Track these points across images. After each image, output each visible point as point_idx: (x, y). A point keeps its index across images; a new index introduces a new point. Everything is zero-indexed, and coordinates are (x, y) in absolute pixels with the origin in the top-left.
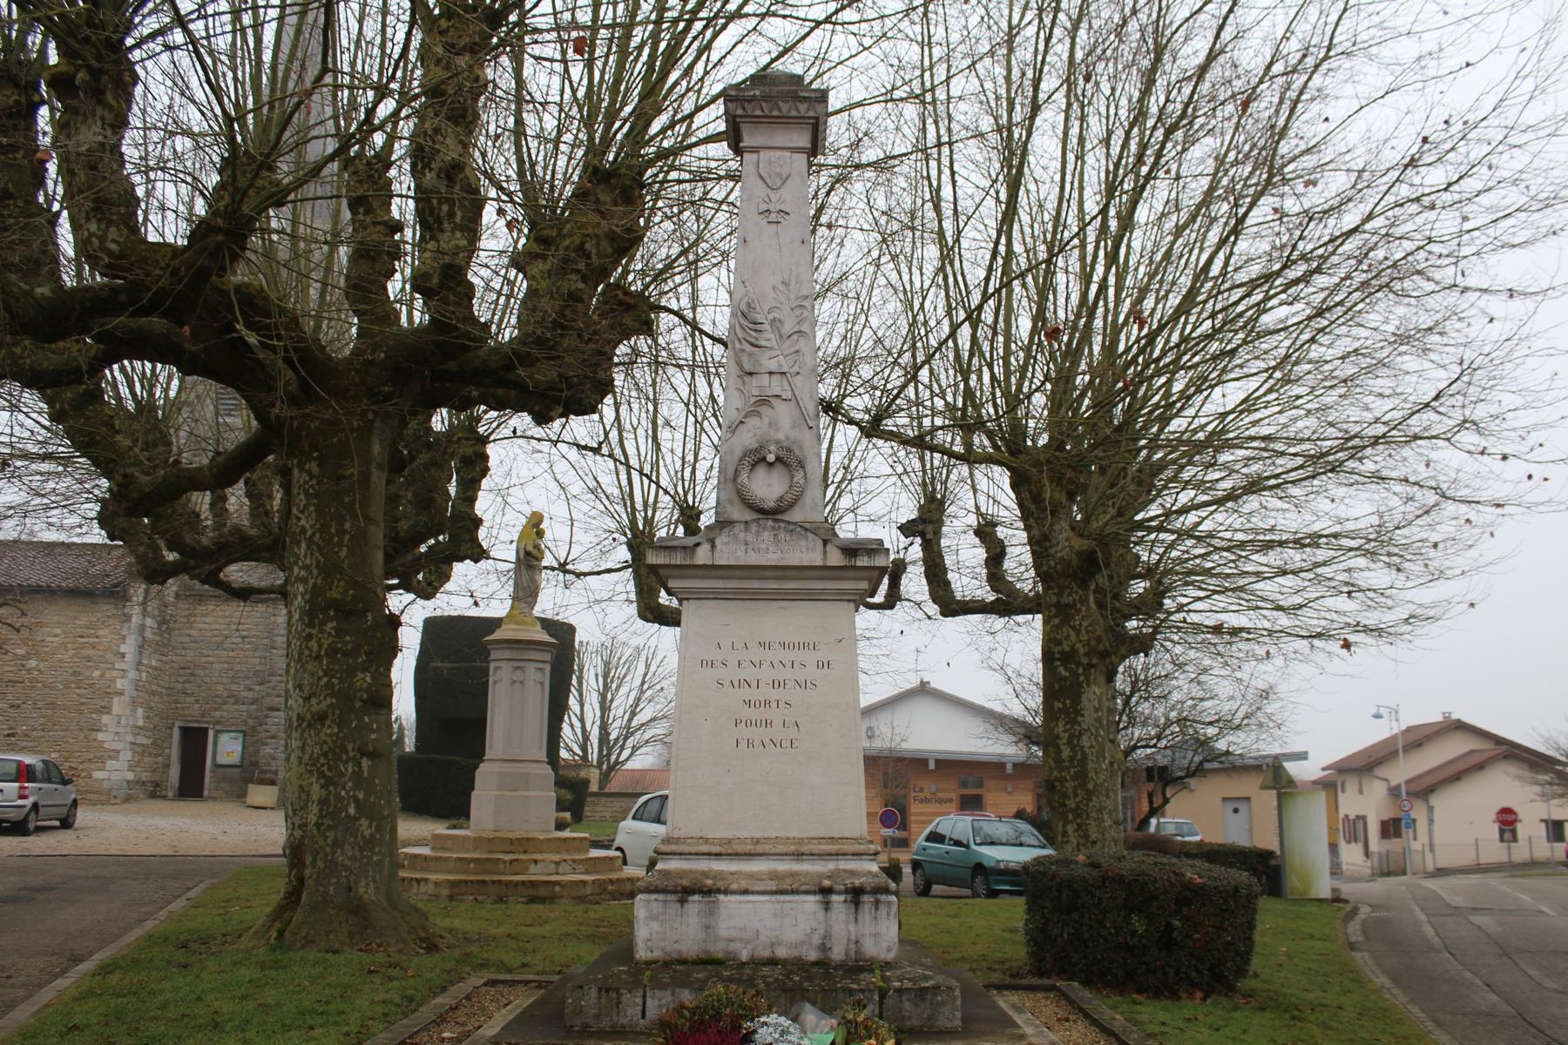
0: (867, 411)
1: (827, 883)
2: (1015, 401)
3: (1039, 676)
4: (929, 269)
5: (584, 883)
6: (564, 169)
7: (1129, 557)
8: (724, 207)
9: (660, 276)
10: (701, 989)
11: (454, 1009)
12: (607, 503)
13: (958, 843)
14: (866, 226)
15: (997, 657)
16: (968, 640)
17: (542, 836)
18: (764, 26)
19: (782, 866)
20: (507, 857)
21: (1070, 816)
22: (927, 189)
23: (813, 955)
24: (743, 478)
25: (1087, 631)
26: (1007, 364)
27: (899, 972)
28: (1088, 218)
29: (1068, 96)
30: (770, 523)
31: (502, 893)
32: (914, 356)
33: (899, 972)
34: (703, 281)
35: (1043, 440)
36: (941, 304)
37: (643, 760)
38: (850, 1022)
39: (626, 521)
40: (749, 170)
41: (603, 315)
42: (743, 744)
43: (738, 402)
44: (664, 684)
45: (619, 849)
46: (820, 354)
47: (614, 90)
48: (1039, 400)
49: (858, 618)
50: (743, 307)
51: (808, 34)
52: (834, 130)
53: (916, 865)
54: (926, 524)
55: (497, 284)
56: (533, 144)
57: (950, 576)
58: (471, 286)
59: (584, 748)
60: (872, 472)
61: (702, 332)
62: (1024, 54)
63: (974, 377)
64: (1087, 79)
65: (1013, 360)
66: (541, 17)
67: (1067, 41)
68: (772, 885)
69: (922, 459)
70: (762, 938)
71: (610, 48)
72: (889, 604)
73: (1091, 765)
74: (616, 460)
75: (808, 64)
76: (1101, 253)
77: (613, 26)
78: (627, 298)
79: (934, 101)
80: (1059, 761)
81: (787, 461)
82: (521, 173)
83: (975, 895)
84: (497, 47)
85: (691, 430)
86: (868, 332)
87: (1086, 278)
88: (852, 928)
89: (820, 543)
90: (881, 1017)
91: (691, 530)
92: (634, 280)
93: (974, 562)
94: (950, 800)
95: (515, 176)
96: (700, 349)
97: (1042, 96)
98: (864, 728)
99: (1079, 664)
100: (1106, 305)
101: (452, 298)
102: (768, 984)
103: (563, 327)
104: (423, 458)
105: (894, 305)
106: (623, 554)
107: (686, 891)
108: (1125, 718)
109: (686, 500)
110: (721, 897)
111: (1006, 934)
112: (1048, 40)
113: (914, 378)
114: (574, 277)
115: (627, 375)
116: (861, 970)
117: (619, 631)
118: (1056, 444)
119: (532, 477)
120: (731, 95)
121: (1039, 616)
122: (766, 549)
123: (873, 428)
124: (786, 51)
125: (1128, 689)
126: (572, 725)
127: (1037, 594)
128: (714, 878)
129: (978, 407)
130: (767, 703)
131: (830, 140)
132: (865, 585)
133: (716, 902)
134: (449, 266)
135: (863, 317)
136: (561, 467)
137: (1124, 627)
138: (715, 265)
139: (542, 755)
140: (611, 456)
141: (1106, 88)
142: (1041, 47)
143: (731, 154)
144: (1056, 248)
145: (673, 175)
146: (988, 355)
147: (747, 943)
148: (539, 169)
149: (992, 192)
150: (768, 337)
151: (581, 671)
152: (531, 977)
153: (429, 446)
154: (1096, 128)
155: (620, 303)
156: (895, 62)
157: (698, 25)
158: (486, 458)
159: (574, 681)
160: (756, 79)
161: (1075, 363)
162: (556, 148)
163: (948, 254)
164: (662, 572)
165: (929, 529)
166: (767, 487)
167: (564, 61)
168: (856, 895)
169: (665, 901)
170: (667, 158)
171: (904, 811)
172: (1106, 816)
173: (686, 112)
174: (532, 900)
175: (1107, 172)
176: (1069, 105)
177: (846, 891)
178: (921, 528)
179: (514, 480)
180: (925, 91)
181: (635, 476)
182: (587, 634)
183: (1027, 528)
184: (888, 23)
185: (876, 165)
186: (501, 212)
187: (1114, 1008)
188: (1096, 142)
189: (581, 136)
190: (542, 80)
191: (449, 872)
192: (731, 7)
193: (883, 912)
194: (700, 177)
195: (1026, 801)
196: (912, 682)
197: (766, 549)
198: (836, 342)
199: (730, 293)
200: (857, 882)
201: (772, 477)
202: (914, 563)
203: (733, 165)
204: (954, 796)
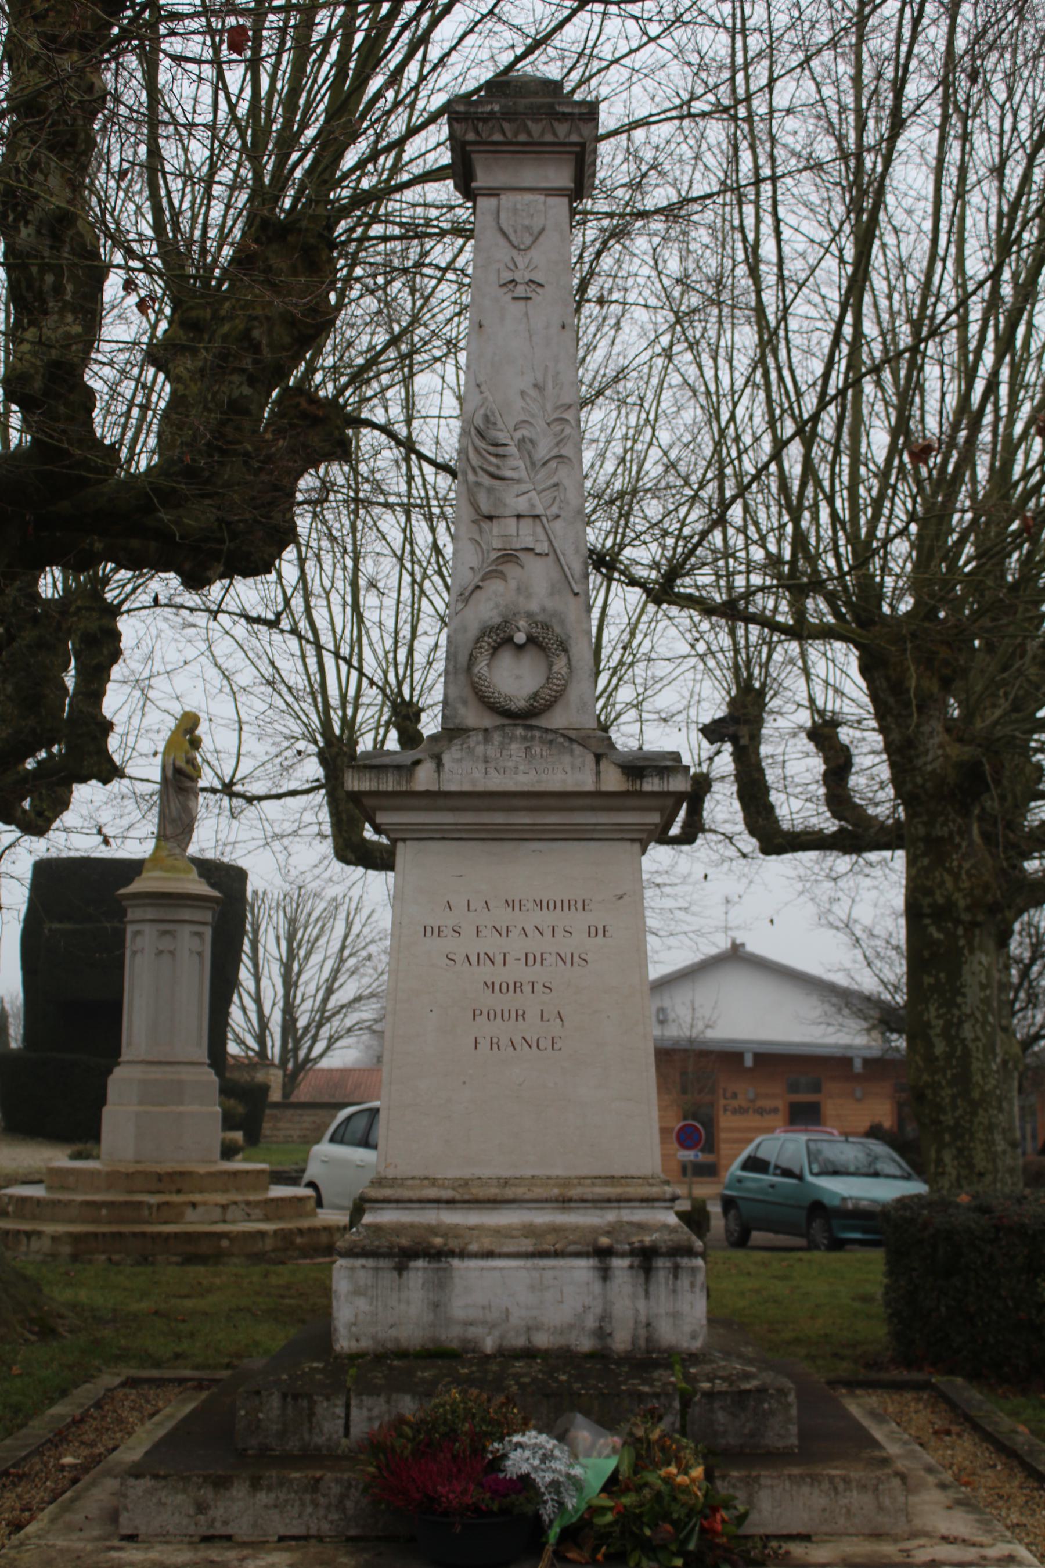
0: (655, 565)
1: (604, 1241)
3: (901, 936)
4: (743, 362)
5: (262, 1234)
6: (220, 219)
7: (1028, 769)
8: (450, 276)
9: (359, 377)
10: (429, 1395)
11: (78, 1422)
12: (290, 699)
13: (787, 1173)
14: (653, 301)
15: (841, 911)
16: (799, 886)
17: (202, 1169)
19: (542, 1218)
20: (153, 1199)
21: (947, 1137)
22: (739, 245)
23: (586, 1344)
24: (481, 666)
25: (970, 876)
26: (854, 496)
27: (708, 1368)
28: (971, 286)
29: (944, 106)
30: (520, 731)
31: (148, 1250)
32: (721, 489)
33: (708, 1368)
34: (423, 382)
35: (906, 605)
36: (760, 410)
37: (344, 1056)
38: (639, 1440)
39: (316, 722)
41: (279, 432)
42: (484, 1044)
43: (472, 558)
44: (373, 949)
45: (312, 1185)
46: (588, 484)
47: (290, 104)
48: (900, 547)
49: (645, 860)
50: (479, 421)
52: (607, 159)
53: (728, 1204)
54: (740, 724)
55: (127, 388)
56: (176, 185)
57: (774, 797)
58: (90, 393)
59: (261, 1039)
60: (662, 651)
61: (421, 456)
62: (881, 43)
63: (807, 515)
64: (973, 78)
65: (862, 491)
67: (944, 23)
68: (527, 1245)
69: (732, 633)
70: (514, 1320)
71: (282, 43)
72: (688, 837)
73: (976, 1065)
74: (300, 637)
75: (569, 63)
76: (991, 334)
78: (313, 409)
79: (749, 119)
80: (930, 1059)
81: (544, 642)
82: (158, 226)
83: (812, 1246)
84: (119, 39)
85: (406, 593)
86: (655, 453)
87: (969, 374)
88: (641, 1304)
89: (590, 759)
90: (683, 1433)
91: (410, 738)
92: (323, 382)
93: (808, 777)
94: (775, 1111)
95: (149, 233)
96: (418, 480)
97: (907, 106)
98: (654, 1010)
99: (958, 922)
100: (997, 409)
101: (62, 409)
102: (522, 1386)
103: (223, 452)
104: (29, 635)
105: (692, 413)
106: (313, 769)
107: (404, 1253)
108: (1022, 995)
109: (400, 693)
110: (456, 1262)
111: (857, 1305)
112: (916, 21)
113: (721, 521)
114: (236, 378)
115: (315, 515)
116: (656, 1364)
117: (309, 877)
118: (923, 611)
119: (185, 665)
120: (459, 111)
121: (900, 853)
123: (663, 591)
124: (537, 44)
125: (1027, 955)
126: (243, 1008)
127: (897, 820)
128: (445, 1235)
129: (813, 559)
130: (518, 986)
131: (600, 175)
132: (655, 818)
133: (449, 1269)
134: (57, 364)
135: (648, 431)
136: (224, 647)
137: (1023, 870)
138: (436, 359)
139: (202, 1054)
140: (295, 631)
141: (999, 91)
142: (907, 33)
143: (457, 199)
144: (925, 328)
145: (377, 230)
146: (826, 484)
147: (493, 1326)
148: (185, 225)
149: (833, 248)
150: (515, 465)
151: (256, 931)
152: (188, 1373)
153: (35, 619)
154: (984, 149)
155: (304, 415)
156: (694, 59)
158: (117, 636)
159: (247, 947)
161: (952, 495)
162: (208, 190)
163: (769, 339)
164: (368, 802)
165: (744, 731)
166: (515, 679)
168: (646, 1258)
169: (377, 1269)
170: (367, 204)
172: (998, 1137)
173: (396, 136)
174: (189, 1259)
175: (1000, 215)
176: (946, 117)
177: (632, 1253)
178: (732, 729)
179: (158, 667)
180: (738, 102)
181: (329, 661)
182: (263, 877)
183: (882, 730)
185: (669, 213)
186: (129, 286)
187: (1014, 1414)
188: (983, 171)
189: (243, 172)
190: (187, 92)
191: (71, 1221)
193: (684, 1282)
194: (413, 232)
195: (882, 1111)
196: (721, 944)
198: (610, 466)
199: (459, 398)
200: (647, 1240)
201: (522, 662)
202: (722, 778)
203: (463, 214)
204: (780, 1104)
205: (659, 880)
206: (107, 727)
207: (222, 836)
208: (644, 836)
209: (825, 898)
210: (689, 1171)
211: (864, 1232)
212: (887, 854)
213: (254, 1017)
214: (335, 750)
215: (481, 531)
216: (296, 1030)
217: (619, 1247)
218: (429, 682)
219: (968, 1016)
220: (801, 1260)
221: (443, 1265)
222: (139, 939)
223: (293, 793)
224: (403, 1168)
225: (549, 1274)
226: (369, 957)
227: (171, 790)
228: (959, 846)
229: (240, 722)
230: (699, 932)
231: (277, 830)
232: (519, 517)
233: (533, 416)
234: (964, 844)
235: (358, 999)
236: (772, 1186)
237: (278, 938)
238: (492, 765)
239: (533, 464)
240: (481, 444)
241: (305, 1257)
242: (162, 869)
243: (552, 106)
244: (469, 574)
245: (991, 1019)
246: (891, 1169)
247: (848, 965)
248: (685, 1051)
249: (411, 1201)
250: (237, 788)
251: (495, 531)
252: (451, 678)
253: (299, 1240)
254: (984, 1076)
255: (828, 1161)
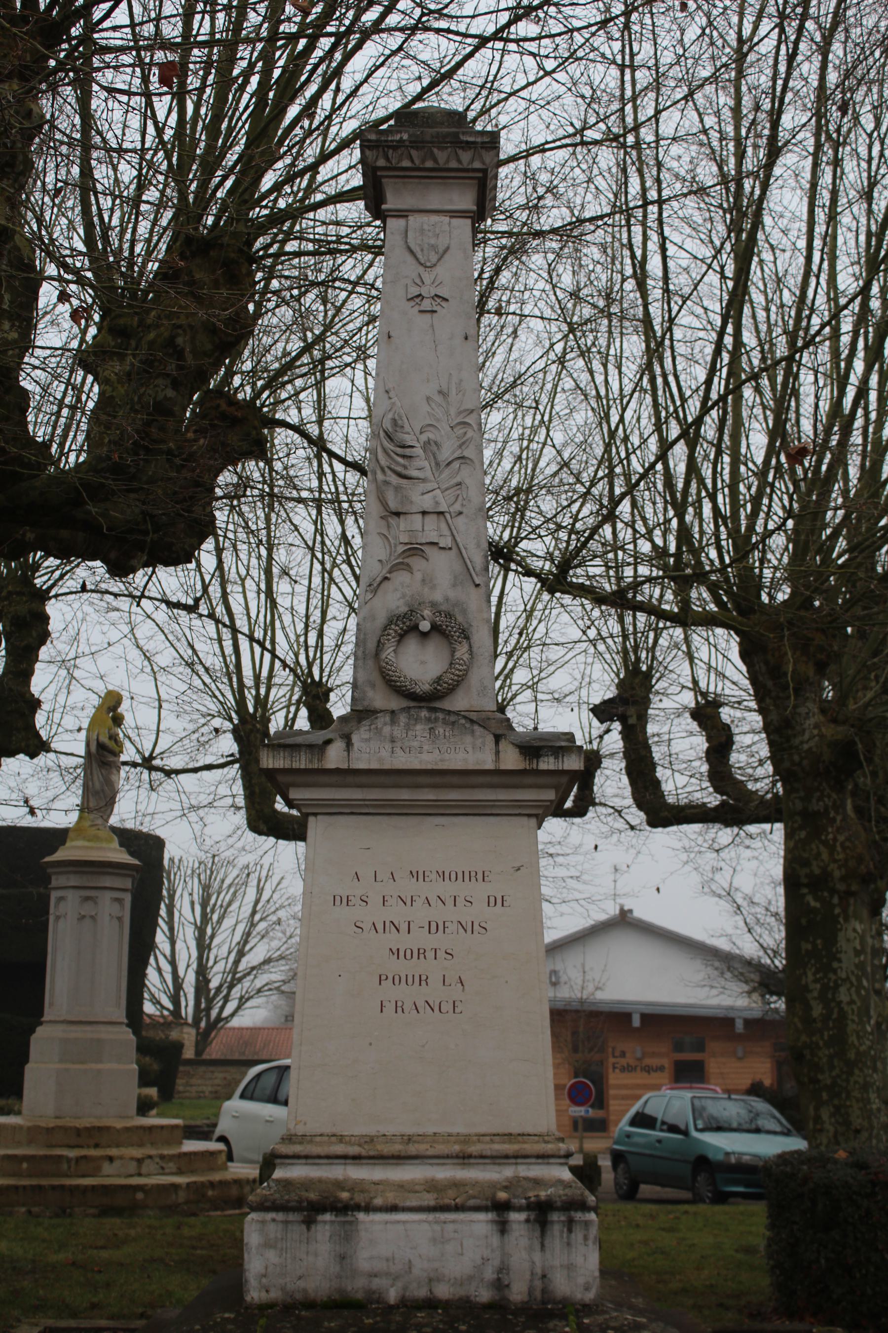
0: (550, 557)
1: (502, 1195)
2: (743, 545)
3: (780, 904)
4: (631, 369)
5: (175, 1187)
6: (146, 238)
9: (274, 382)
13: (673, 1129)
14: (548, 313)
15: (723, 880)
16: (684, 857)
17: (119, 1124)
18: (414, 45)
19: (443, 1173)
20: (72, 1153)
21: (825, 1096)
22: (628, 261)
23: (484, 1295)
24: (388, 653)
27: (600, 1319)
29: (817, 135)
30: (424, 713)
31: (66, 1202)
33: (600, 1319)
34: (333, 385)
36: (647, 412)
37: (253, 1015)
40: (394, 241)
42: (389, 1008)
43: (380, 551)
44: (282, 914)
45: (223, 1139)
47: (213, 129)
48: (778, 541)
49: (542, 835)
50: (388, 425)
51: (471, 55)
53: (618, 1158)
54: (628, 706)
55: (58, 389)
56: (106, 203)
57: (660, 773)
58: (25, 394)
59: (175, 1000)
60: (555, 636)
61: (332, 455)
62: (759, 77)
64: (843, 109)
65: (742, 488)
66: (115, 24)
67: (817, 59)
68: (429, 1199)
69: (621, 620)
70: (416, 1271)
72: (579, 811)
73: (851, 1026)
74: (218, 621)
77: (209, 44)
79: (637, 145)
81: (447, 630)
82: (89, 240)
84: (55, 71)
85: (317, 580)
86: (549, 453)
88: (537, 1257)
89: (490, 739)
91: (320, 718)
93: (692, 754)
94: (661, 1069)
97: (783, 136)
99: (833, 891)
103: (147, 450)
105: (584, 415)
106: (228, 745)
109: (310, 674)
110: (361, 1216)
111: (739, 1256)
112: (791, 58)
113: (611, 517)
114: (160, 381)
116: (552, 1315)
117: (223, 846)
119: (107, 642)
120: (370, 138)
121: (779, 826)
122: (421, 748)
123: (556, 582)
126: (159, 970)
127: (776, 795)
128: (351, 1190)
129: (696, 552)
132: (550, 795)
133: (355, 1223)
135: (543, 431)
136: (145, 630)
140: (212, 616)
142: (782, 68)
144: (799, 340)
146: (709, 482)
147: (396, 1278)
148: (114, 236)
150: (421, 466)
151: (172, 897)
157: (325, 43)
158: (46, 619)
159: (163, 912)
160: (404, 115)
161: (825, 494)
163: (655, 350)
164: (281, 778)
166: (420, 664)
167: (148, 95)
168: (541, 1212)
169: (286, 1222)
171: (600, 1081)
172: (873, 1096)
174: (106, 1211)
176: (818, 146)
177: (529, 1207)
179: (83, 648)
182: (179, 845)
183: (761, 711)
184: (578, 39)
186: (64, 297)
192: (371, 16)
193: (578, 1235)
194: (327, 248)
195: (762, 1069)
196: (611, 910)
197: (421, 748)
198: (507, 464)
200: (543, 1194)
201: (427, 656)
202: (612, 755)
204: (666, 1062)
205: (551, 851)
206: (36, 704)
207: (141, 807)
208: (540, 811)
209: (708, 868)
210: (580, 1126)
211: (746, 1186)
212: (767, 827)
213: (169, 978)
214: (249, 727)
215: (389, 527)
216: (209, 990)
217: (515, 1201)
218: (337, 664)
219: (844, 980)
220: (686, 1212)
221: (349, 1218)
222: (62, 904)
223: (209, 767)
224: (312, 1126)
225: (450, 1227)
226: (279, 922)
227: (94, 765)
228: (834, 820)
229: (159, 700)
230: (589, 900)
231: (194, 802)
232: (424, 513)
233: (438, 420)
234: (839, 818)
235: (267, 961)
236: (659, 1141)
237: (192, 903)
238: (399, 744)
239: (437, 464)
240: (386, 444)
241: (216, 1209)
242: (84, 839)
243: (456, 135)
244: (378, 566)
245: (865, 983)
246: (772, 1125)
247: (730, 931)
248: (577, 1011)
249: (319, 1157)
250: (157, 762)
251: (402, 528)
252: (360, 663)
253: (210, 1193)
254: (859, 1037)
255: (711, 1117)
